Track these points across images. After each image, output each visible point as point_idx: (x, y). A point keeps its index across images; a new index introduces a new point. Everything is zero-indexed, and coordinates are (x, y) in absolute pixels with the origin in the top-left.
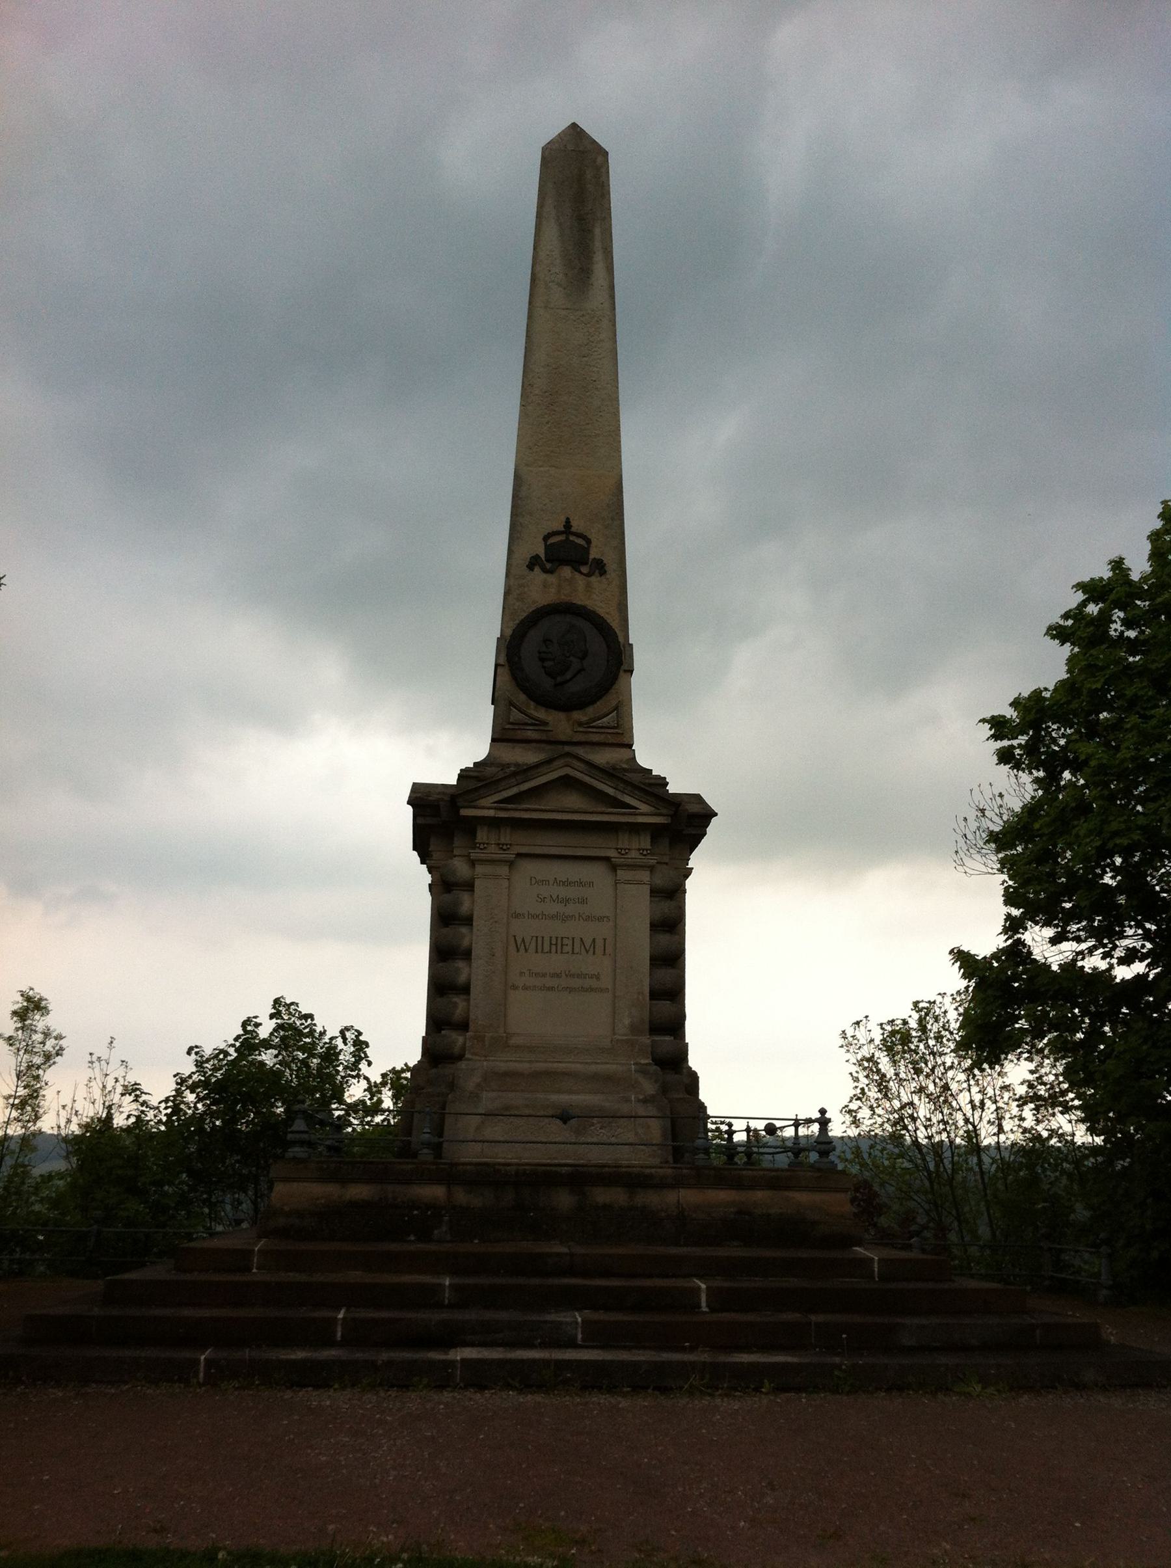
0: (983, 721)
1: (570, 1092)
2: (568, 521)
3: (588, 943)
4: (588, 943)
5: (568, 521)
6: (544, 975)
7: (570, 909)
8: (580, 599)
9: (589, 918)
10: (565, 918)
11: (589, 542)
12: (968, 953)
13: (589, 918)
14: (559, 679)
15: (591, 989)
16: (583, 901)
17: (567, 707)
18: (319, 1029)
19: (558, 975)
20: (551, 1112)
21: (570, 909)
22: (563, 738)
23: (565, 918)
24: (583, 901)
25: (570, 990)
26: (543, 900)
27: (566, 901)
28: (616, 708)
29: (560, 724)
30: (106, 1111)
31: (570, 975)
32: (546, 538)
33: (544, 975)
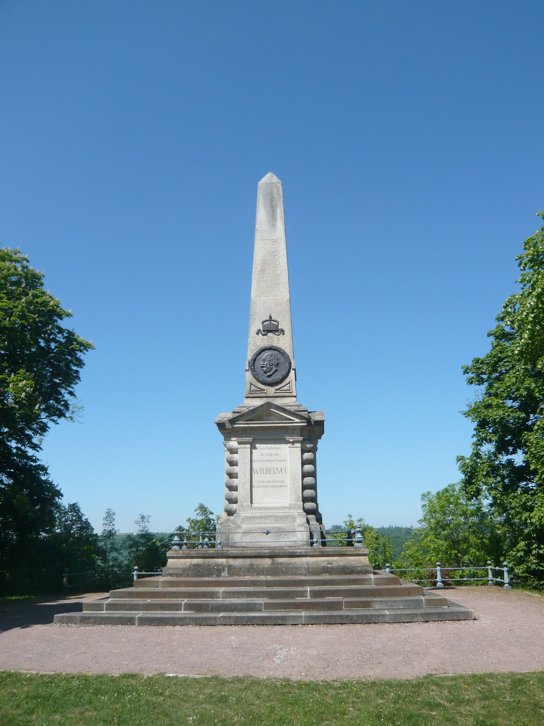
0: (489, 335)
1: (265, 523)
2: (270, 316)
3: (279, 470)
4: (279, 470)
5: (270, 316)
6: (264, 482)
7: (273, 458)
8: (275, 344)
9: (279, 461)
10: (271, 461)
11: (278, 323)
12: (89, 523)
13: (279, 461)
14: (268, 374)
15: (281, 486)
16: (277, 454)
17: (272, 384)
18: (88, 349)
19: (269, 482)
20: (263, 531)
21: (273, 458)
22: (271, 396)
23: (271, 461)
24: (277, 454)
25: (274, 487)
26: (263, 455)
27: (271, 455)
28: (289, 383)
29: (271, 390)
30: (296, 445)
31: (273, 481)
32: (263, 323)
33: (264, 482)
